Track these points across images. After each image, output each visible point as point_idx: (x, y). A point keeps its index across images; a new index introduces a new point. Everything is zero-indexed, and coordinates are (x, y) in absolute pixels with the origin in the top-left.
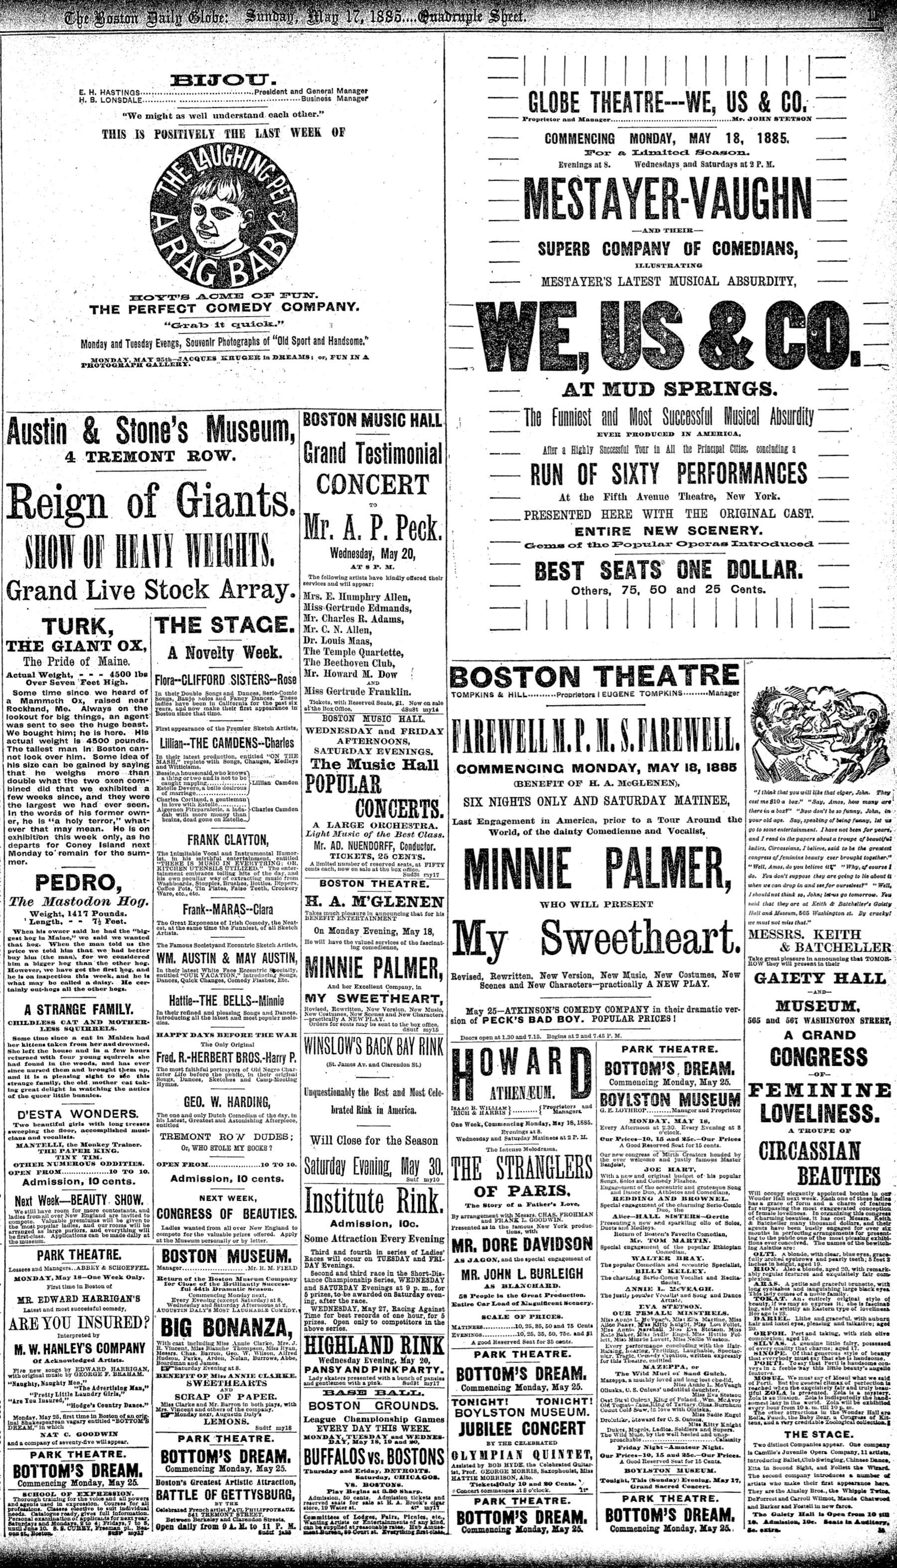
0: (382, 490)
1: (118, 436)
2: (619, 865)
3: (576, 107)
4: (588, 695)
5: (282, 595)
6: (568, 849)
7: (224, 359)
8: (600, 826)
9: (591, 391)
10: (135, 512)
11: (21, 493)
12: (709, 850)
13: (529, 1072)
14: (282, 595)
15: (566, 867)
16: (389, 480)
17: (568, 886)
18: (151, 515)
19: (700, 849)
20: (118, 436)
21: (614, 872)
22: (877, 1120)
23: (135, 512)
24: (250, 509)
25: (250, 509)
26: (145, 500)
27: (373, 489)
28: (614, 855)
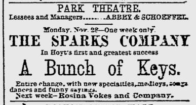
0: (86, 73)
5: (163, 73)
7: (110, 96)
10: (112, 72)
11: (51, 64)
14: (163, 73)
16: (36, 38)
18: (119, 74)
20: (122, 62)
22: (179, 73)
23: (112, 72)
24: (74, 72)
25: (74, 72)
26: (117, 68)
27: (81, 73)
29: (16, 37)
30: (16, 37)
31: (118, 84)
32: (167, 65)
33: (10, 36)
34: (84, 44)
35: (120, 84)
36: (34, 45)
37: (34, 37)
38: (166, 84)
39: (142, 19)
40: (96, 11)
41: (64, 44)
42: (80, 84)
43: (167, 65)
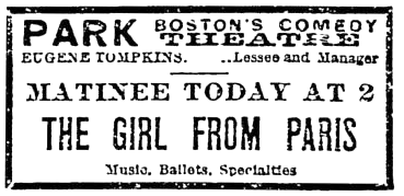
1: (354, 125)
2: (297, 133)
3: (84, 140)
4: (389, 44)
6: (86, 119)
8: (157, 178)
9: (341, 94)
10: (120, 143)
12: (210, 119)
13: (257, 120)
15: (86, 133)
16: (160, 87)
17: (86, 148)
19: (204, 119)
20: (354, 125)
21: (293, 138)
28: (294, 124)
29: (340, 88)
30: (88, 87)
31: (242, 169)
32: (55, 119)
33: (77, 85)
34: (40, 89)
35: (266, 171)
36: (136, 97)
37: (136, 86)
38: (208, 171)
39: (278, 58)
40: (84, 99)
41: (340, 97)
42: (145, 171)
43: (55, 119)
